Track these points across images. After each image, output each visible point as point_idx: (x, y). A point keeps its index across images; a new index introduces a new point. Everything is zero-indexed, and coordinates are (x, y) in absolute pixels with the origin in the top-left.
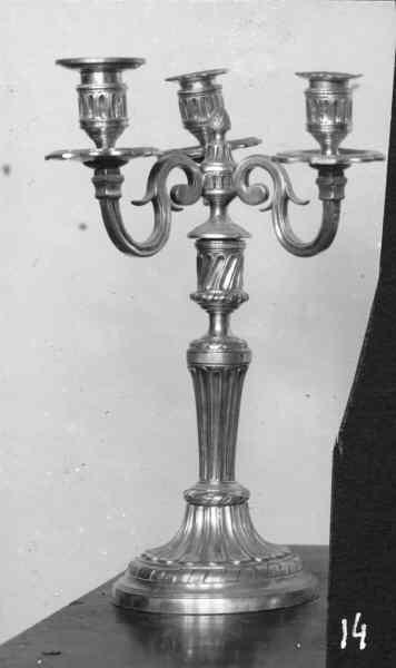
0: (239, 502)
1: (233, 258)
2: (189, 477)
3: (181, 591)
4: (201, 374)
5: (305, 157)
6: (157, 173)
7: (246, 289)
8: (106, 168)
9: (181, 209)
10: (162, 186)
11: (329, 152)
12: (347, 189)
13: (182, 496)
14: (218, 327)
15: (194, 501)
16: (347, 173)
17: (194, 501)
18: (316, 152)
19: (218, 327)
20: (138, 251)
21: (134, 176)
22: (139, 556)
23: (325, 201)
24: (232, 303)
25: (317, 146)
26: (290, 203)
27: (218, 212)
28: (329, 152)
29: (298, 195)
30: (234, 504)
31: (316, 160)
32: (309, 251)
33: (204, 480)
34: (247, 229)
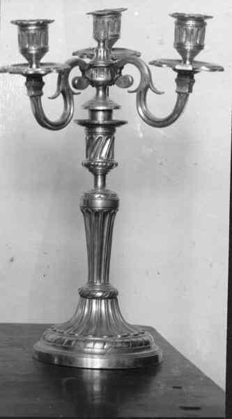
0: (112, 297)
1: (107, 139)
2: (83, 282)
3: (82, 352)
4: (87, 208)
5: (171, 64)
6: (63, 74)
7: (116, 159)
8: (35, 83)
9: (79, 93)
10: (67, 83)
11: (188, 62)
12: (195, 87)
13: (77, 292)
14: (100, 183)
15: (86, 296)
16: (196, 76)
17: (86, 296)
18: (180, 61)
19: (100, 183)
20: (50, 126)
21: (51, 82)
22: (10, 65)
23: (179, 93)
24: (109, 166)
25: (180, 58)
26: (149, 91)
27: (101, 93)
28: (188, 62)
29: (155, 86)
30: (109, 298)
31: (178, 67)
32: (156, 124)
33: (91, 283)
34: (120, 104)
